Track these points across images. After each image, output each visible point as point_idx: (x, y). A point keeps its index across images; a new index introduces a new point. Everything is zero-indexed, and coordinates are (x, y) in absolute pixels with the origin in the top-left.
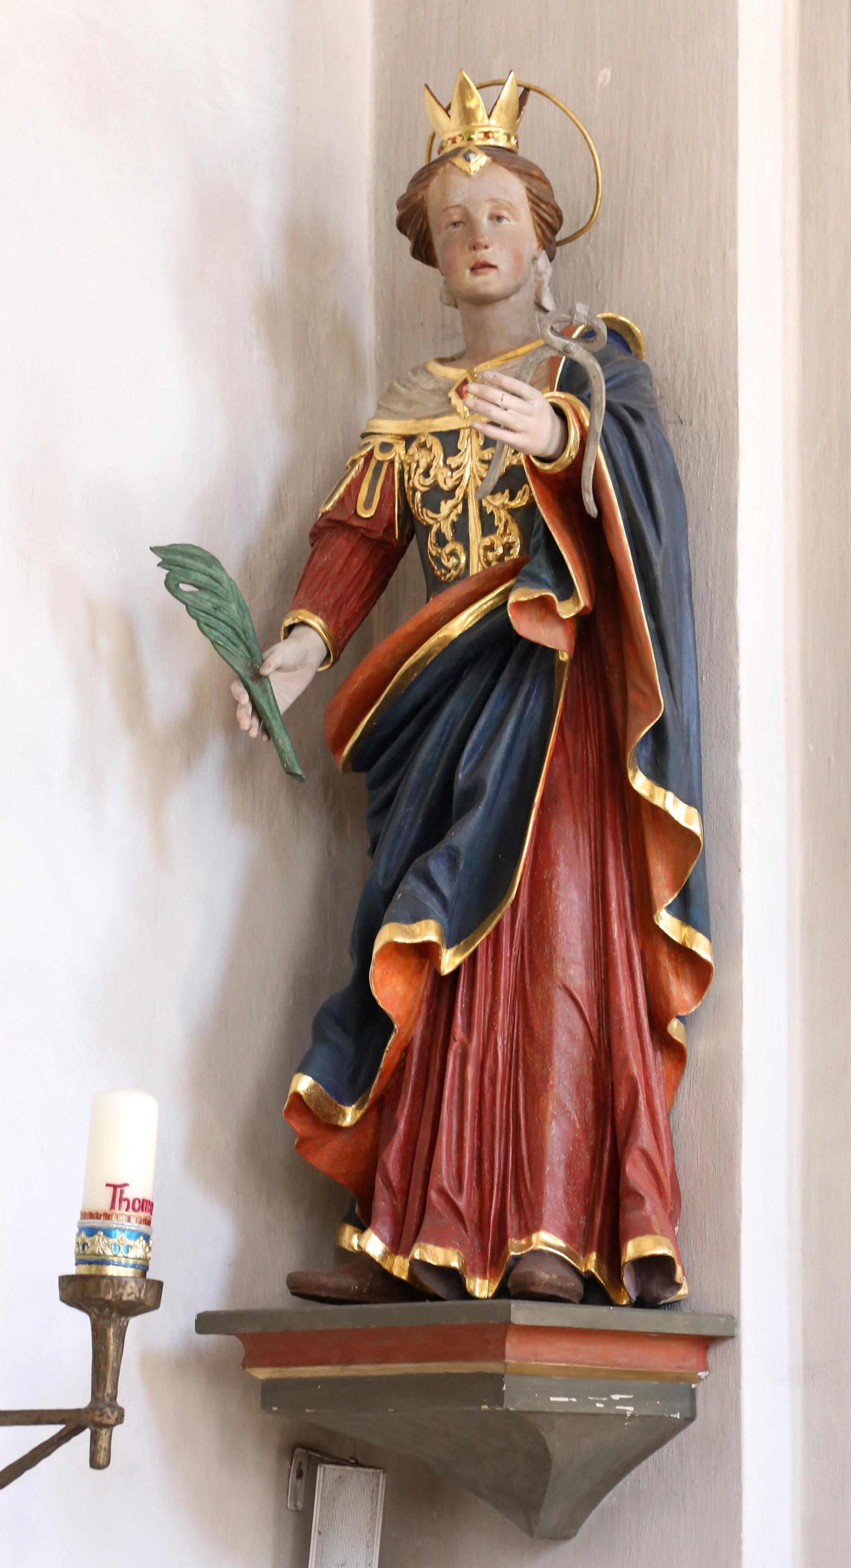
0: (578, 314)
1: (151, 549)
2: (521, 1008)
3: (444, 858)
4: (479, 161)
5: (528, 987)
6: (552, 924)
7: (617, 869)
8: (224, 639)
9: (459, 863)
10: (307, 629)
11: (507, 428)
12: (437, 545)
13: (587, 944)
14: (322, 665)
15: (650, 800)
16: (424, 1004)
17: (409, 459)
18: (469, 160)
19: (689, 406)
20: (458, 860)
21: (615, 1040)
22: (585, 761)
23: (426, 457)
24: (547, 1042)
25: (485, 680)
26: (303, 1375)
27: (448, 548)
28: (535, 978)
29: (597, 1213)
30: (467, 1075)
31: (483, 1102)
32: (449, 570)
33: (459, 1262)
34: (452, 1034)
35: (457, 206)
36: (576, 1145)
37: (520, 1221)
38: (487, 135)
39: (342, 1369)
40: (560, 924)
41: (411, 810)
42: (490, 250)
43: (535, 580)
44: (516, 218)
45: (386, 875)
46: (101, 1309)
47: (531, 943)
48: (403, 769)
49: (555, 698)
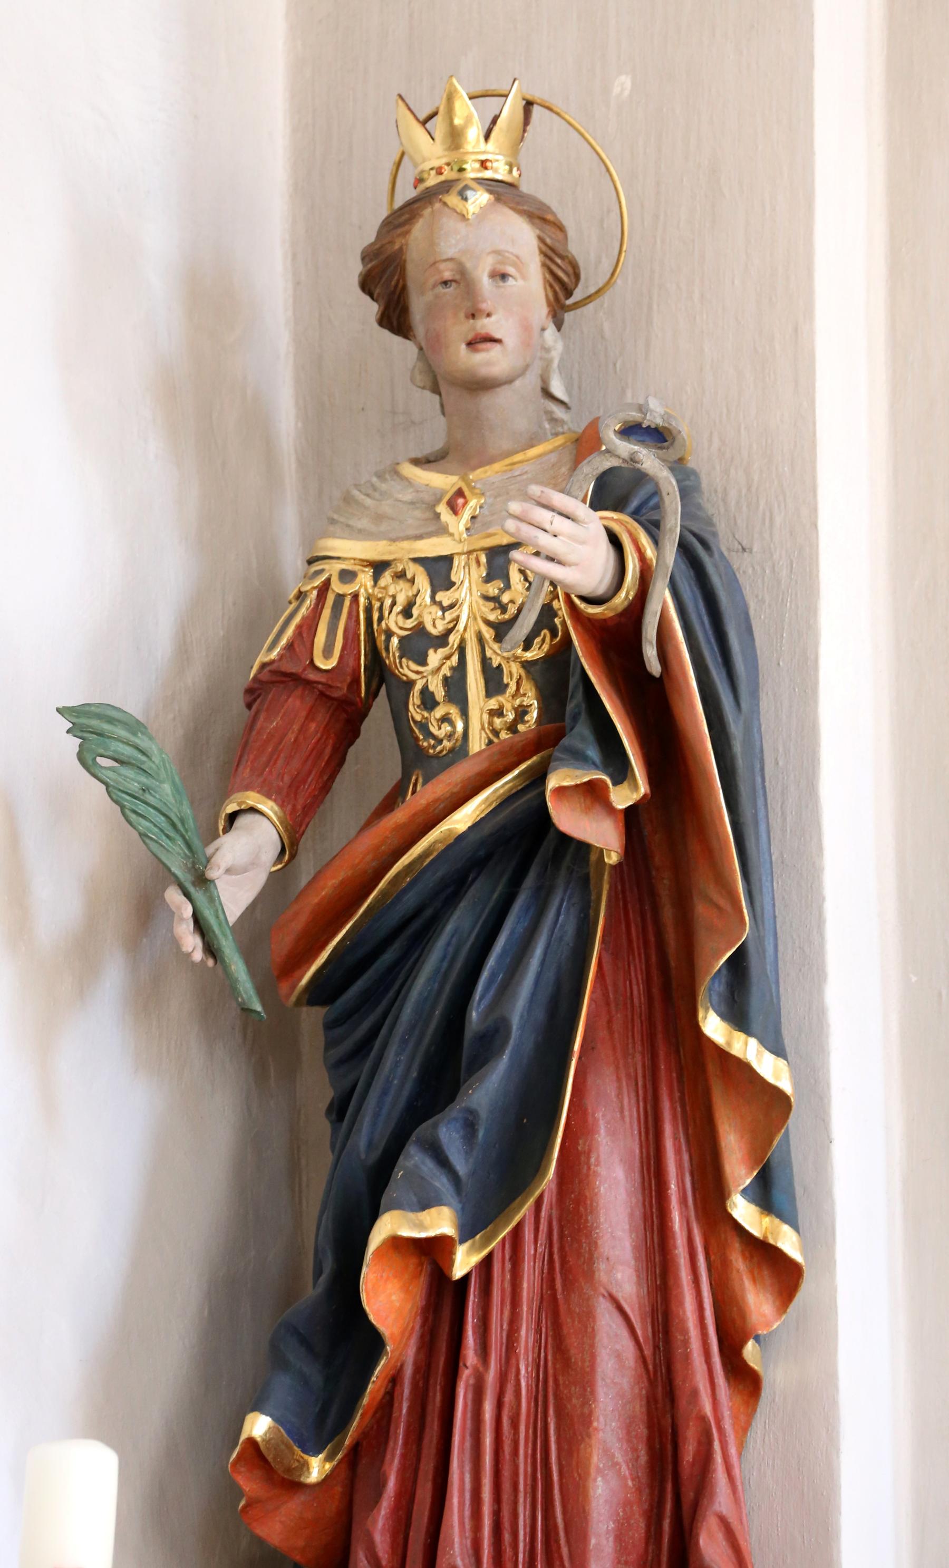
0: (652, 411)
1: (58, 710)
2: (549, 1323)
3: (458, 1125)
4: (479, 199)
5: (559, 1296)
6: (591, 1212)
7: (676, 1138)
8: (156, 830)
9: (477, 1130)
10: (257, 817)
11: (560, 563)
12: (422, 706)
13: (637, 1237)
15: (727, 1049)
17: (380, 592)
18: (466, 199)
19: (747, 527)
21: (678, 1366)
23: (406, 591)
24: (588, 1370)
25: (500, 888)
27: (439, 712)
30: (484, 1415)
32: (440, 741)
35: (451, 260)
36: (628, 1509)
38: (484, 164)
41: (402, 1058)
42: (493, 318)
43: (578, 758)
44: (524, 278)
45: (370, 1145)
47: (562, 1236)
49: (592, 913)
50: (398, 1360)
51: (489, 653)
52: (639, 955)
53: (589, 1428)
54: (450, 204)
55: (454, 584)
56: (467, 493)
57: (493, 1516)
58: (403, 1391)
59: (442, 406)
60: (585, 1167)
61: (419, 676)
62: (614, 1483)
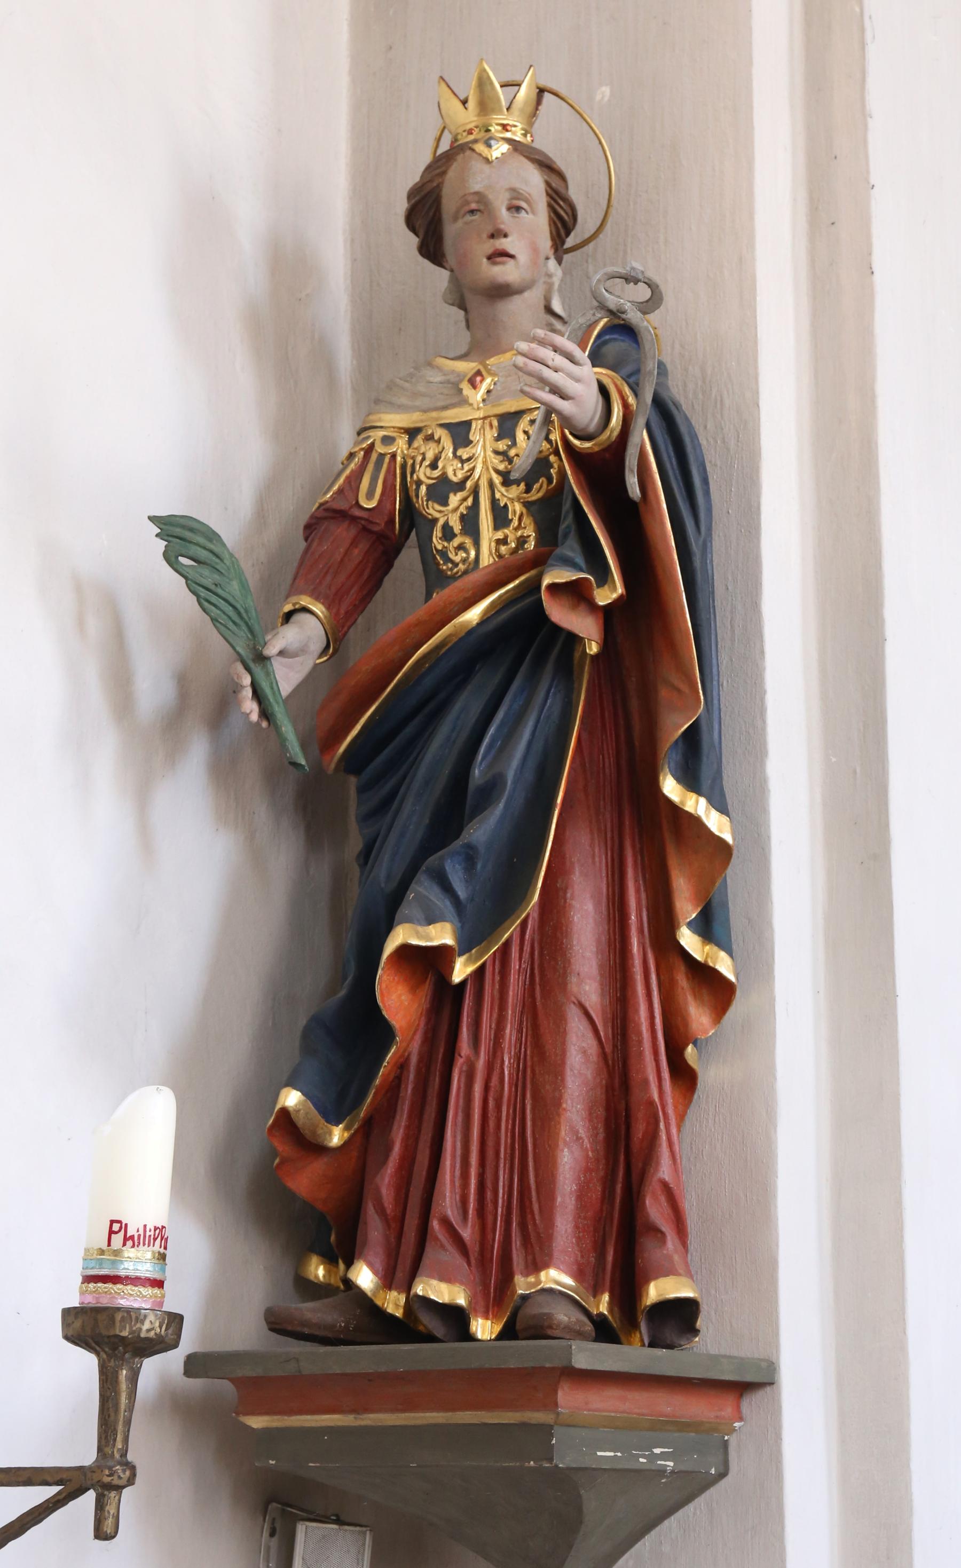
1: (150, 518)
2: (529, 1024)
8: (225, 617)
12: (443, 538)
14: (320, 656)
15: (681, 806)
16: (423, 1018)
17: (413, 452)
18: (490, 146)
19: (702, 410)
20: (476, 860)
22: (601, 766)
23: (434, 449)
26: (307, 1425)
27: (456, 542)
28: (547, 993)
29: (609, 1250)
31: (486, 1125)
32: (456, 565)
33: (465, 1300)
34: (457, 1051)
37: (526, 1256)
39: (355, 1418)
40: (575, 936)
41: (417, 808)
42: (509, 239)
43: (569, 563)
44: (534, 213)
45: (389, 877)
46: (114, 1349)
47: (541, 954)
48: (405, 767)
50: (405, 1051)
51: (498, 496)
52: (611, 735)
53: (559, 1109)
54: (477, 150)
55: (472, 442)
56: (484, 373)
57: (479, 1177)
58: (409, 1076)
59: (467, 321)
60: (563, 901)
61: (442, 515)
62: (578, 1153)
